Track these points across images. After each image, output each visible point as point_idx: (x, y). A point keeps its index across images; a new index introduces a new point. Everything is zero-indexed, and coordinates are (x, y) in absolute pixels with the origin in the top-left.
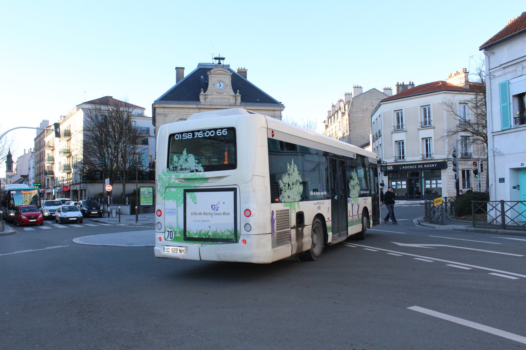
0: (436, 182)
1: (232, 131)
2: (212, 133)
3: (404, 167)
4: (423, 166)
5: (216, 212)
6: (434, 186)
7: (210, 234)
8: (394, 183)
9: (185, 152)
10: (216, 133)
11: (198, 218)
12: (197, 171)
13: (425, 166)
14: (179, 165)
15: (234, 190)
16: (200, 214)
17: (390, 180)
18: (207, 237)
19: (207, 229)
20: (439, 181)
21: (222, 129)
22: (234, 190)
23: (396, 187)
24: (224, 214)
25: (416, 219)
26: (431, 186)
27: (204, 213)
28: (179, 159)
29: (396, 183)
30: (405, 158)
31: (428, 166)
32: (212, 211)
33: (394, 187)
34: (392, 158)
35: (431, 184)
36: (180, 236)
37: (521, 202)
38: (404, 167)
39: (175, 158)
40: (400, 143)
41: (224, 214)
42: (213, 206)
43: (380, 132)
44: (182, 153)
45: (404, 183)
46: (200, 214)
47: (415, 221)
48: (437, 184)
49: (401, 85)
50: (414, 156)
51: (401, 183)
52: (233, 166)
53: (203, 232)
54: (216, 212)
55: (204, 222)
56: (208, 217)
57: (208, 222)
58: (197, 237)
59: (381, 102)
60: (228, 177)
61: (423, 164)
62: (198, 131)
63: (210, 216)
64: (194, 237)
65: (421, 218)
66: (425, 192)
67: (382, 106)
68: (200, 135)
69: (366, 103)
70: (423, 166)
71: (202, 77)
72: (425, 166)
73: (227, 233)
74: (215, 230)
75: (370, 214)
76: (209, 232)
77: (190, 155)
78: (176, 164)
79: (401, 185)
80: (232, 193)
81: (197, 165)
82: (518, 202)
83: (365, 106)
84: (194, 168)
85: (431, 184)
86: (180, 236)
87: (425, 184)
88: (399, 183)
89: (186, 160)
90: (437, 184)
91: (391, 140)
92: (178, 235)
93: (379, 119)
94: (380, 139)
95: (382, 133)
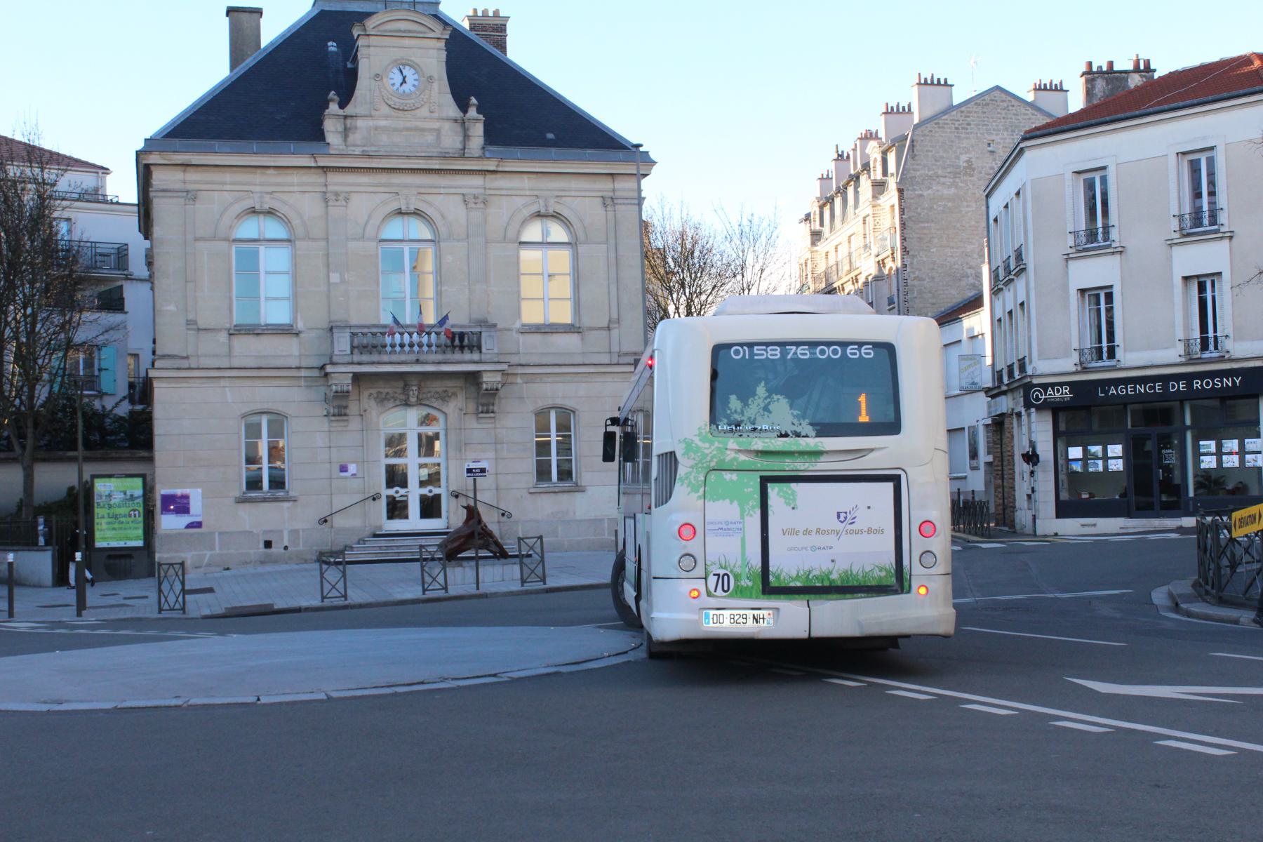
0: (1242, 445)
1: (887, 350)
2: (835, 352)
5: (849, 527)
6: (1231, 461)
7: (834, 576)
8: (1075, 452)
12: (798, 435)
14: (745, 418)
15: (895, 480)
16: (807, 532)
17: (1062, 437)
18: (826, 584)
20: (1251, 444)
21: (861, 344)
22: (895, 480)
23: (1085, 466)
24: (870, 531)
25: (1165, 589)
26: (1220, 462)
27: (818, 531)
28: (746, 404)
29: (1085, 451)
30: (1119, 353)
32: (839, 526)
33: (1077, 467)
34: (1067, 355)
36: (750, 584)
38: (1113, 391)
39: (734, 403)
40: (1099, 299)
41: (870, 531)
42: (842, 516)
43: (1019, 256)
44: (754, 394)
45: (1116, 450)
46: (807, 532)
47: (1159, 596)
48: (1242, 452)
49: (1100, 72)
50: (1153, 344)
51: (1105, 451)
53: (815, 573)
56: (830, 540)
57: (829, 551)
58: (799, 584)
59: (1024, 139)
60: (882, 451)
64: (792, 584)
65: (1184, 586)
66: (1198, 485)
69: (965, 143)
71: (332, 46)
72: (1197, 384)
76: (831, 572)
79: (1105, 458)
80: (890, 486)
81: (796, 421)
83: (964, 157)
85: (1219, 453)
86: (750, 584)
87: (1197, 454)
88: (1096, 449)
89: (766, 409)
90: (1242, 452)
91: (1065, 287)
92: (745, 582)
93: (1017, 206)
94: (1020, 283)
95: (1030, 260)
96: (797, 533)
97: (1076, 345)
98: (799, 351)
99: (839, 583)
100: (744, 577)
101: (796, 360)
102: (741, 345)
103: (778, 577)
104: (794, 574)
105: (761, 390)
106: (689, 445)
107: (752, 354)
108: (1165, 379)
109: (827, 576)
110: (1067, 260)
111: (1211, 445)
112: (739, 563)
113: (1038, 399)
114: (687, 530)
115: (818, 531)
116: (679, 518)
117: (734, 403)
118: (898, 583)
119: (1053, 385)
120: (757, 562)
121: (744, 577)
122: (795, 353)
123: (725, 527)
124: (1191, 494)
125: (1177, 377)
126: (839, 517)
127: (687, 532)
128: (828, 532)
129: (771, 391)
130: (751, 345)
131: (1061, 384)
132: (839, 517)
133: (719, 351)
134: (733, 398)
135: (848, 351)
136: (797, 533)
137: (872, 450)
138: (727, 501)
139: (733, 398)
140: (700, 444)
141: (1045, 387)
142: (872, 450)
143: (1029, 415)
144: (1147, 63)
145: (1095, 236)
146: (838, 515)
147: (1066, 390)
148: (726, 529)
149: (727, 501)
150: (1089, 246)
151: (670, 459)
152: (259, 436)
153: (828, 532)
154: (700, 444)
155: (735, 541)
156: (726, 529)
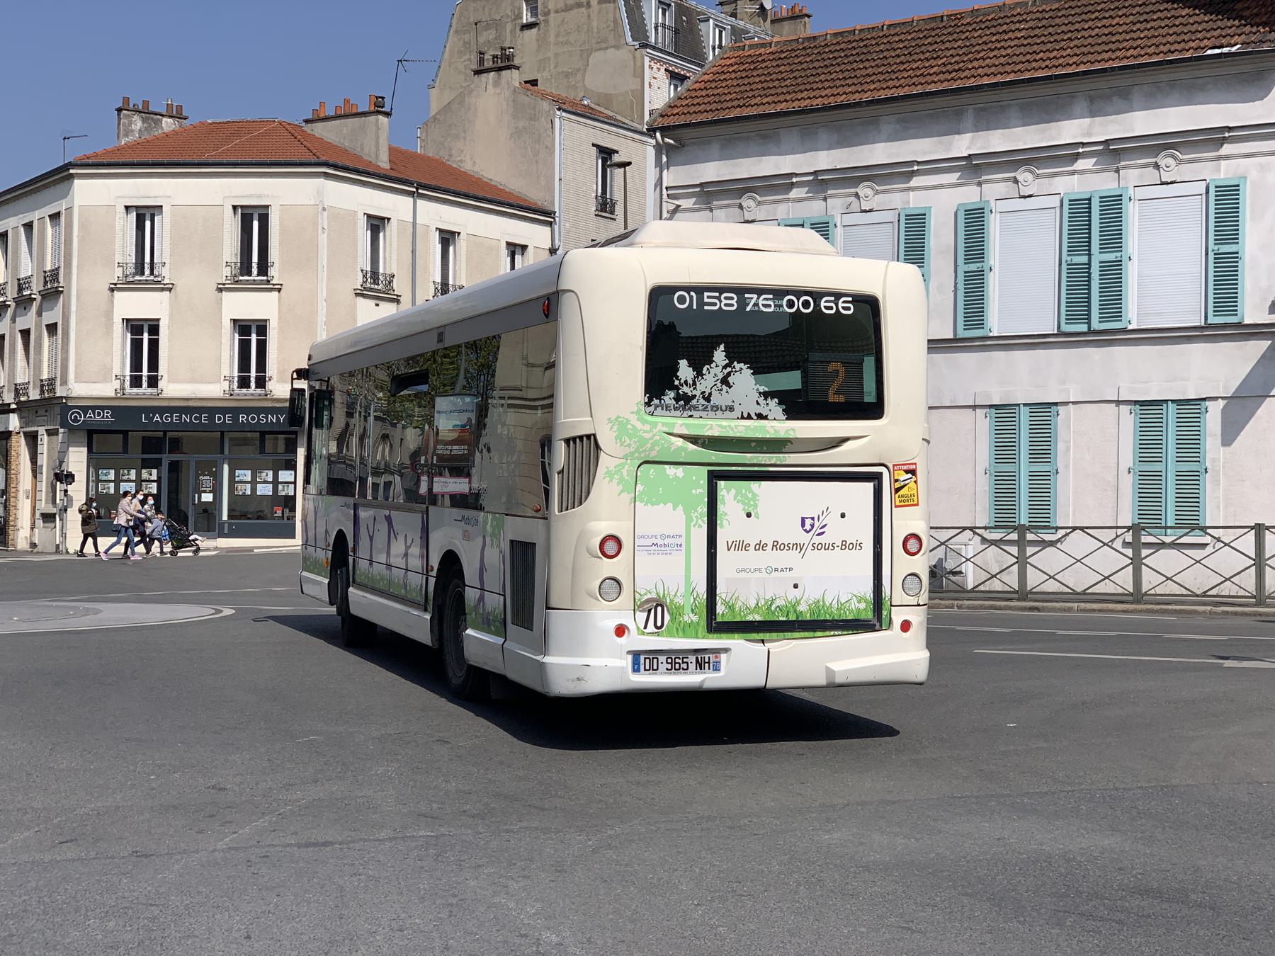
0: (276, 476)
1: (869, 306)
2: (806, 304)
3: (157, 418)
4: (235, 418)
5: (817, 540)
7: (802, 608)
9: (719, 355)
10: (817, 305)
11: (752, 558)
12: (760, 416)
13: (242, 418)
14: (698, 393)
15: (876, 478)
16: (760, 546)
17: (95, 462)
18: (792, 617)
19: (793, 594)
21: (838, 296)
22: (876, 478)
24: (844, 545)
26: (254, 489)
27: (775, 545)
28: (699, 374)
31: (254, 419)
32: (804, 538)
34: (105, 380)
35: (254, 483)
36: (695, 619)
37: (1082, 529)
38: (157, 418)
39: (685, 371)
41: (844, 545)
42: (808, 522)
44: (710, 361)
46: (760, 546)
52: (875, 410)
53: (778, 602)
54: (817, 540)
55: (775, 574)
56: (790, 558)
57: (787, 574)
58: (758, 618)
60: (860, 440)
61: (235, 411)
62: (760, 291)
63: (795, 552)
64: (750, 618)
67: (76, 182)
68: (765, 304)
70: (235, 418)
72: (242, 418)
73: (855, 605)
74: (818, 596)
75: (434, 573)
76: (798, 603)
77: (737, 366)
78: (686, 389)
80: (869, 486)
81: (761, 400)
82: (1074, 529)
84: (754, 410)
85: (254, 483)
86: (695, 619)
87: (159, 481)
89: (725, 381)
91: (109, 314)
92: (689, 617)
96: (745, 547)
97: (117, 371)
98: (761, 302)
99: (808, 617)
100: (688, 610)
101: (757, 313)
102: (688, 289)
103: (731, 608)
104: (752, 604)
105: (719, 355)
106: (620, 423)
107: (701, 303)
108: (211, 411)
109: (793, 606)
110: (112, 290)
111: (246, 475)
112: (682, 590)
113: (76, 420)
114: (611, 545)
115: (775, 545)
116: (602, 527)
117: (685, 371)
118: (872, 619)
119: (93, 408)
120: (702, 589)
121: (688, 610)
122: (756, 305)
123: (660, 542)
124: (225, 517)
125: (224, 411)
126: (803, 525)
127: (611, 547)
128: (789, 547)
129: (732, 357)
130: (700, 290)
131: (103, 408)
132: (803, 525)
133: (659, 295)
134: (683, 363)
135: (823, 304)
136: (745, 547)
137: (846, 440)
138: (670, 505)
139: (683, 363)
140: (639, 425)
141: (85, 409)
142: (846, 440)
143: (32, 439)
144: (180, 108)
145: (143, 272)
146: (803, 520)
147: (107, 414)
148: (661, 546)
149: (670, 505)
150: (137, 278)
151: (587, 445)
152: (257, 378)
153: (789, 547)
154: (639, 425)
155: (678, 558)
156: (661, 546)
